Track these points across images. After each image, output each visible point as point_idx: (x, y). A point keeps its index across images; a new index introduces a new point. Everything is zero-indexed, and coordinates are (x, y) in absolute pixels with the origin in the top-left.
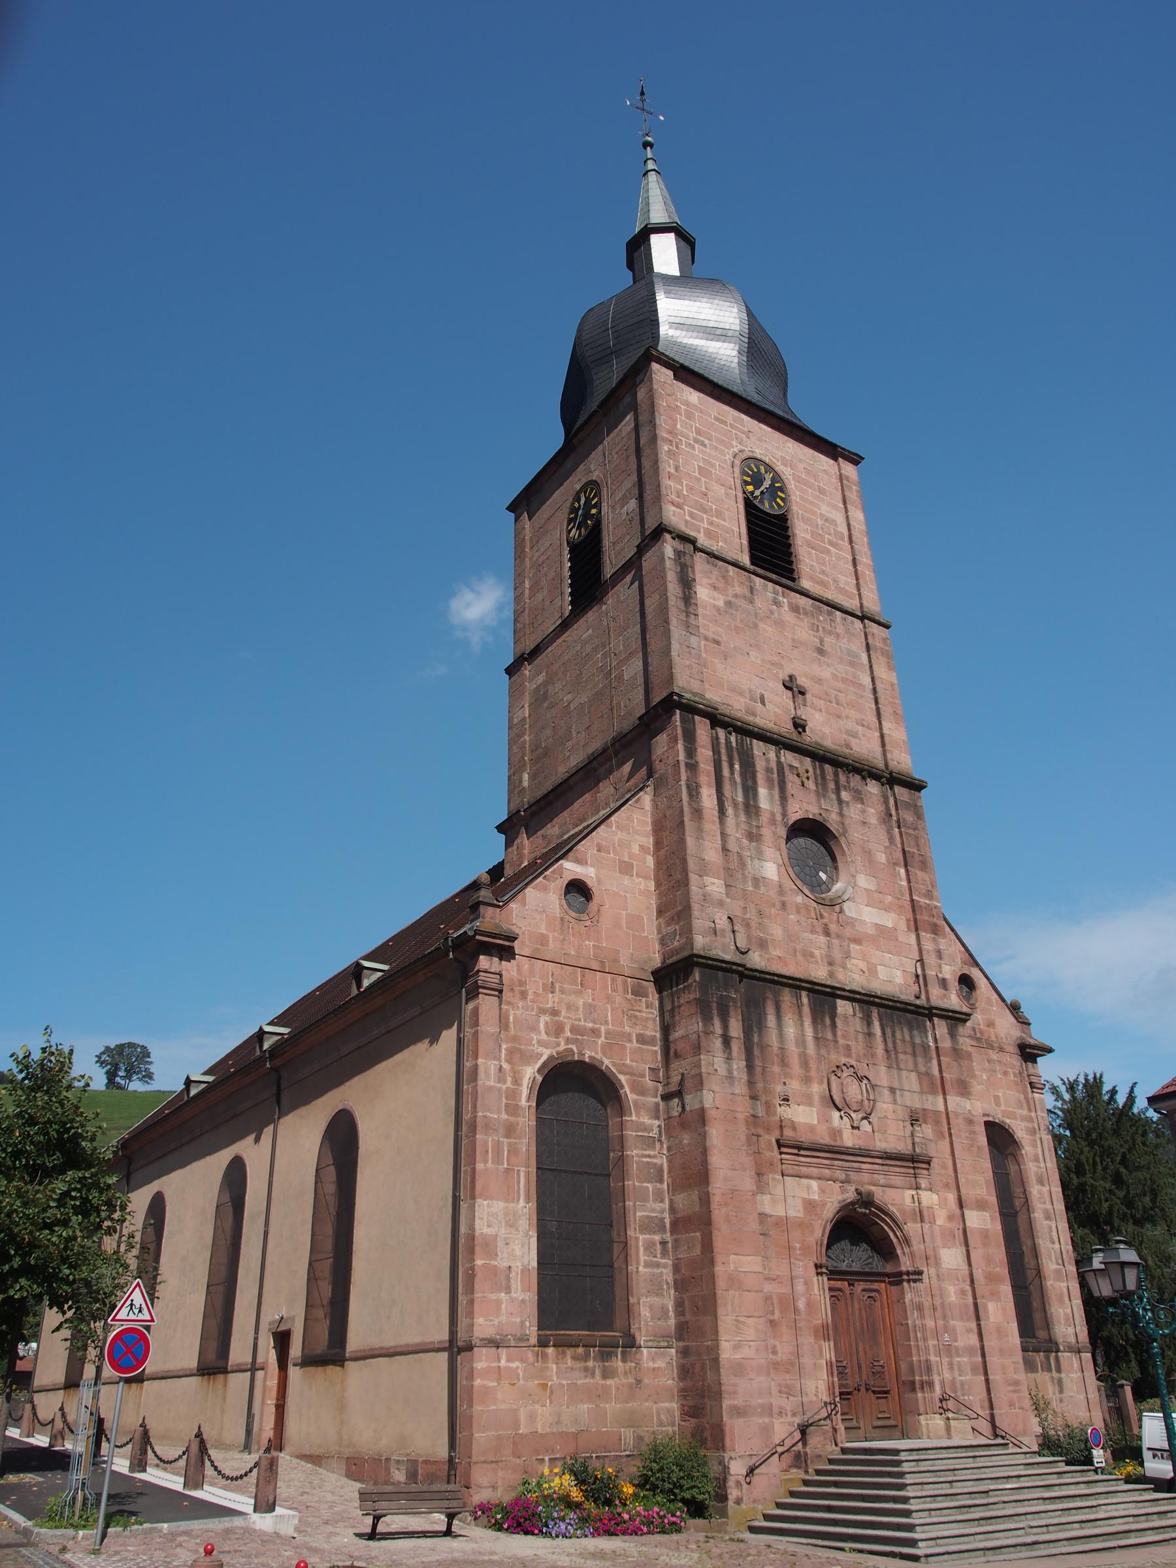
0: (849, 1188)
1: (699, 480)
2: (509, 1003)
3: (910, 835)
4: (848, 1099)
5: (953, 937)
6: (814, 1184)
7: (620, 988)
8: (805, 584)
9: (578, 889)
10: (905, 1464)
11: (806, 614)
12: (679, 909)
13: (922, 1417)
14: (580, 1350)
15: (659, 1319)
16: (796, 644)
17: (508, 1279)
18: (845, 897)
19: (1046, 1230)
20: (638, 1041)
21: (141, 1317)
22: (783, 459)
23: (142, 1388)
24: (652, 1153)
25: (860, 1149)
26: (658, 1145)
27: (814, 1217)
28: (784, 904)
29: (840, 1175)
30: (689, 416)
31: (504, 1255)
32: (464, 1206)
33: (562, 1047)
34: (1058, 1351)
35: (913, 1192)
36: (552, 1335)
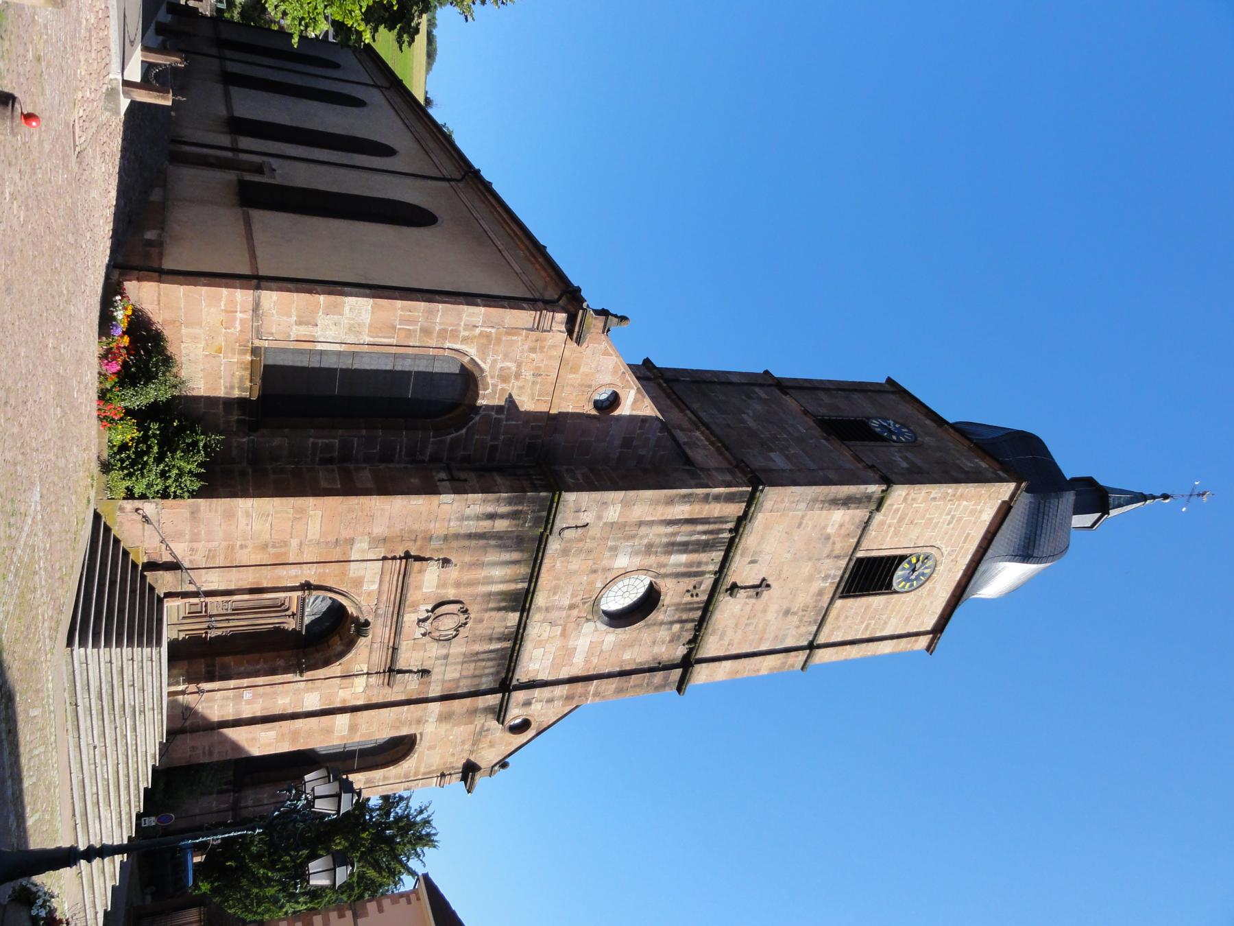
1: (923, 518)
2: (527, 337)
3: (644, 680)
6: (375, 587)
12: (596, 483)
17: (307, 324)
20: (492, 446)
28: (595, 571)
34: (235, 792)
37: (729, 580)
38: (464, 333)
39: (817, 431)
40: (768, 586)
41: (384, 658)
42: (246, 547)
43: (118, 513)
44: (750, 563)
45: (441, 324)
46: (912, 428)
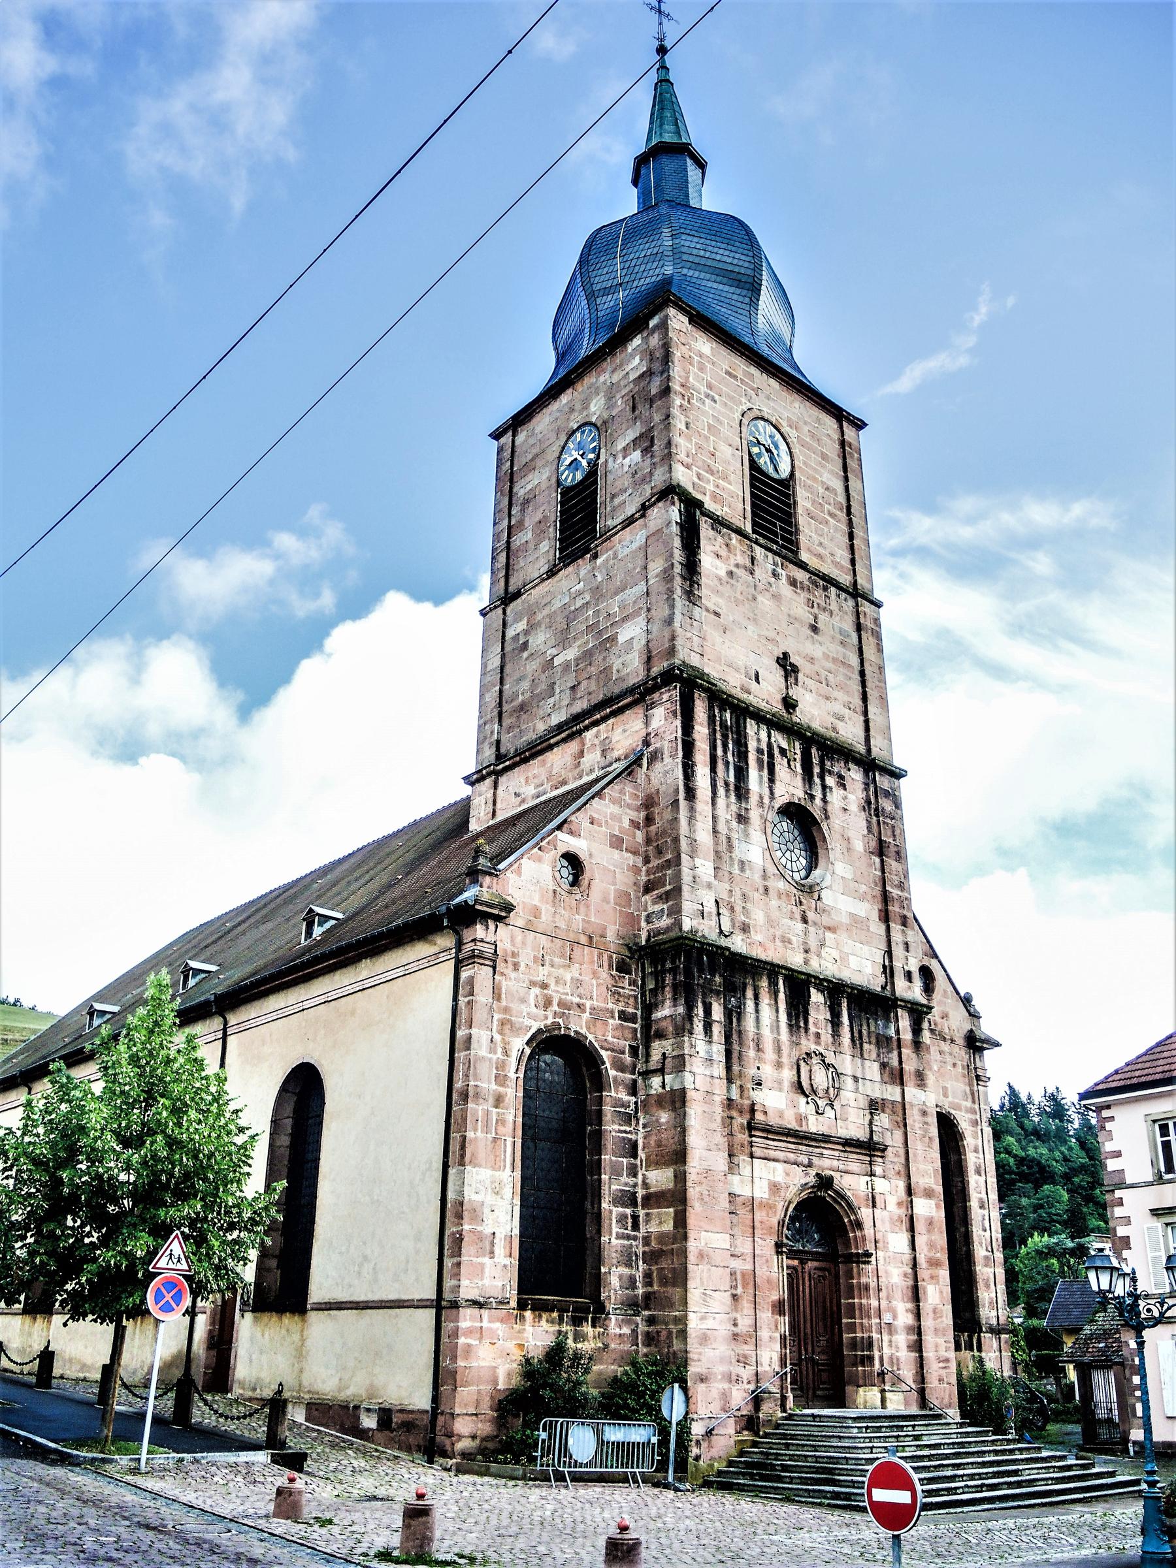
0: (811, 1172)
1: (707, 439)
2: (502, 974)
3: (887, 824)
4: (815, 1086)
5: (917, 927)
7: (606, 964)
8: (804, 556)
9: (573, 861)
10: (924, 1438)
11: (802, 588)
12: (668, 888)
13: (861, 1390)
14: (555, 1314)
15: (627, 1289)
16: (792, 620)
17: (492, 1244)
18: (823, 885)
19: (980, 1219)
20: (620, 1018)
21: (179, 1266)
22: (789, 419)
23: (49, 1322)
24: (628, 1129)
25: (823, 1135)
26: (633, 1122)
27: (777, 1198)
28: (766, 890)
30: (702, 368)
31: (490, 1222)
32: (452, 1172)
33: (549, 1022)
34: (981, 1331)
35: (868, 1178)
36: (529, 1299)
37: (778, 707)
38: (499, 1054)
39: (584, 566)
40: (786, 655)
41: (855, 1156)
42: (735, 1319)
43: (701, 1462)
45: (489, 1082)
46: (575, 426)
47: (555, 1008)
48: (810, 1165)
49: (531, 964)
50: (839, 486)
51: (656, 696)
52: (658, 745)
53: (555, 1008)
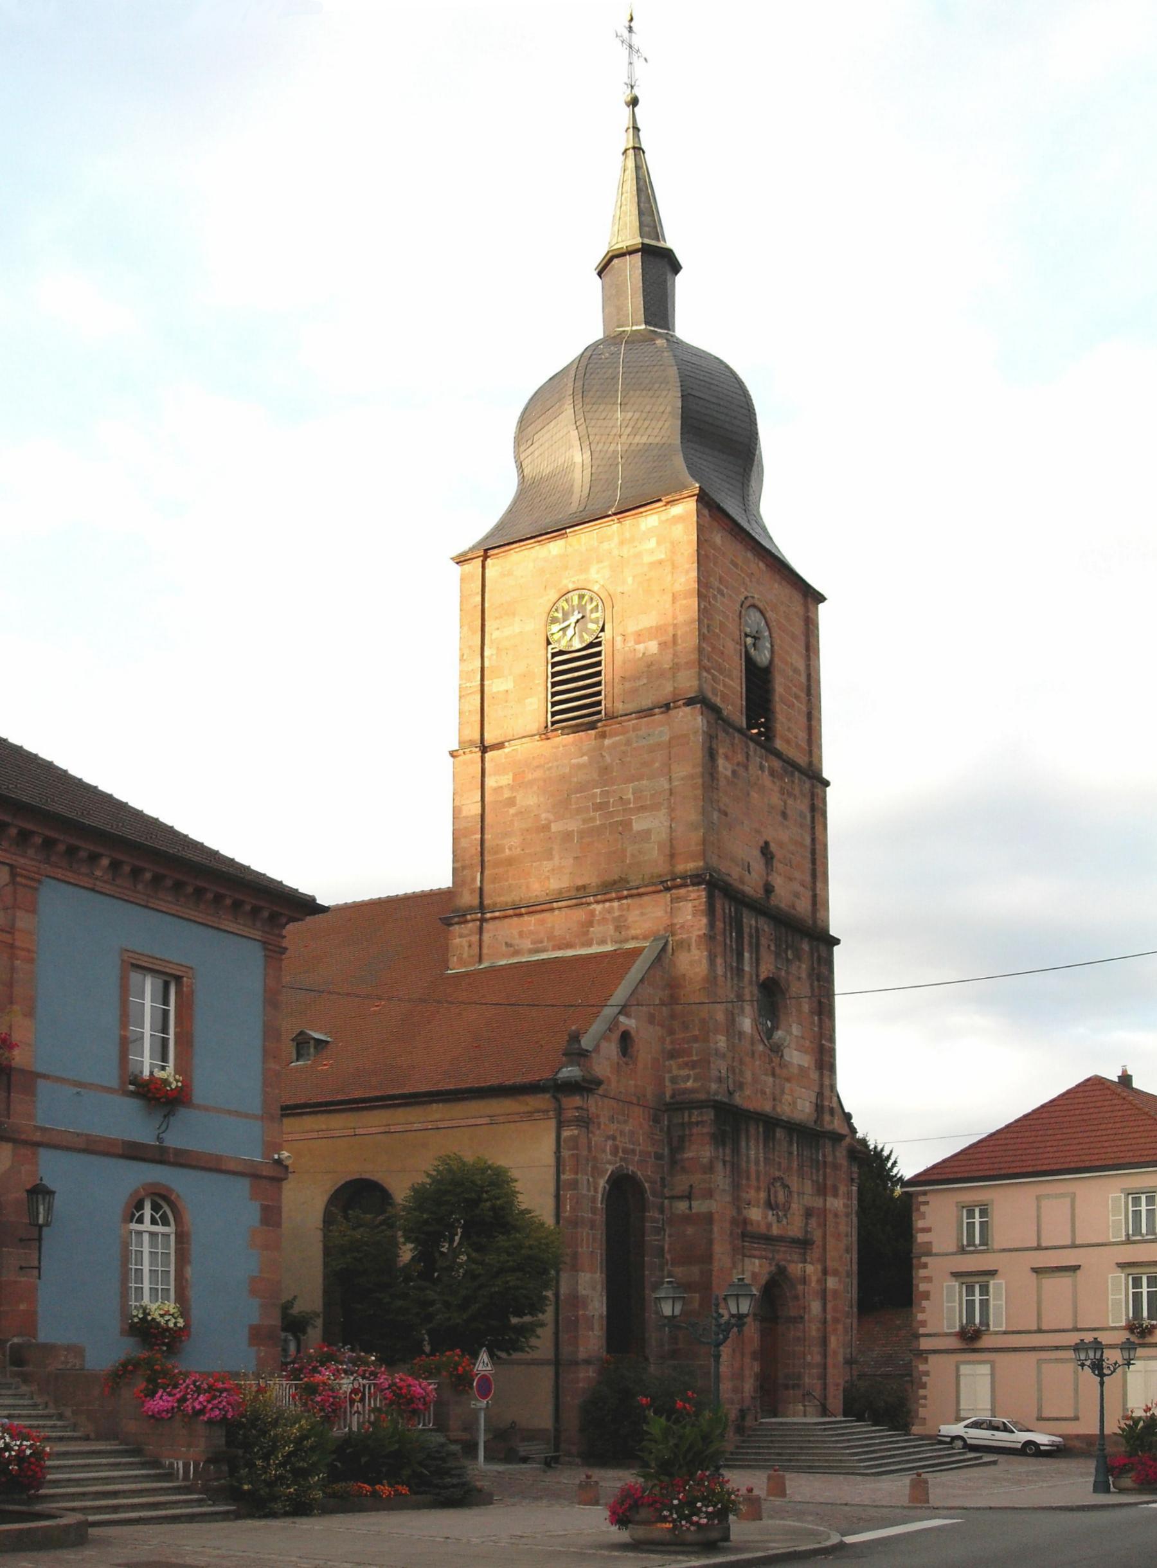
6: (757, 1261)
8: (779, 744)
26: (662, 1233)
29: (770, 1255)
38: (592, 1193)
44: (749, 872)
47: (621, 1154)
48: (773, 1258)
49: (607, 1122)
50: (801, 666)
51: (682, 891)
52: (684, 936)
53: (621, 1154)
